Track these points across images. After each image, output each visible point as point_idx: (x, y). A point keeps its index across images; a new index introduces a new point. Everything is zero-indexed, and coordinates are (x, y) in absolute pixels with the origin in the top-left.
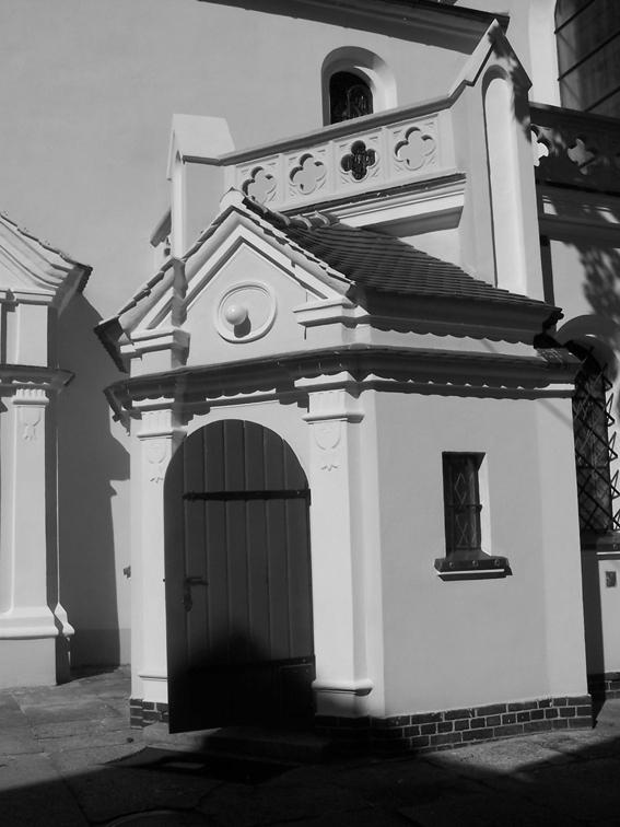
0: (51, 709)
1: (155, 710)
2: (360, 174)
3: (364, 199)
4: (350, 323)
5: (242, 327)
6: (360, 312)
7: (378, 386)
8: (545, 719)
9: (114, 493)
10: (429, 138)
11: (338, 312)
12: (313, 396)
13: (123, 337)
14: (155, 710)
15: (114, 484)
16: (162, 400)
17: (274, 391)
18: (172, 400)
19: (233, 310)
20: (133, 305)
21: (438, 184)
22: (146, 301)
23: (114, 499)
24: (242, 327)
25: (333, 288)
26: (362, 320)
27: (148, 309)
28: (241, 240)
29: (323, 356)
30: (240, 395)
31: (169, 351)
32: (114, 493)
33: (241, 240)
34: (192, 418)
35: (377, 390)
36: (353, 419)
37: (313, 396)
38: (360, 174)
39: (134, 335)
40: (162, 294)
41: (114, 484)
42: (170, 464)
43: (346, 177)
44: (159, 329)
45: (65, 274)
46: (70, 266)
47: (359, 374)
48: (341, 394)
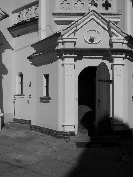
0: (19, 136)
1: (69, 133)
2: (107, 9)
3: (75, 14)
4: (123, 43)
5: (92, 40)
6: (126, 42)
7: (128, 59)
8: (33, 128)
9: (3, 78)
10: (69, 4)
11: (122, 41)
12: (115, 59)
13: (60, 37)
14: (69, 133)
15: (3, 76)
16: (73, 55)
17: (102, 57)
18: (76, 56)
19: (93, 36)
20: (66, 29)
21: (117, 15)
22: (69, 29)
23: (3, 80)
24: (92, 40)
25: (121, 35)
26: (125, 44)
27: (69, 31)
28: (93, 19)
29: (122, 50)
30: (93, 57)
31: (74, 43)
32: (3, 78)
33: (93, 19)
34: (77, 61)
35: (128, 60)
36: (124, 65)
37: (115, 59)
38: (107, 9)
39: (64, 37)
40: (73, 28)
41: (3, 76)
42: (80, 73)
43: (103, 8)
44: (70, 37)
45: (2, 16)
46: (4, 14)
47: (126, 56)
48: (121, 59)
